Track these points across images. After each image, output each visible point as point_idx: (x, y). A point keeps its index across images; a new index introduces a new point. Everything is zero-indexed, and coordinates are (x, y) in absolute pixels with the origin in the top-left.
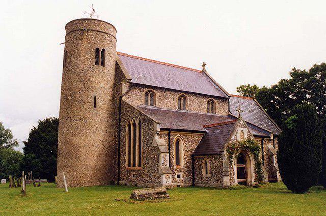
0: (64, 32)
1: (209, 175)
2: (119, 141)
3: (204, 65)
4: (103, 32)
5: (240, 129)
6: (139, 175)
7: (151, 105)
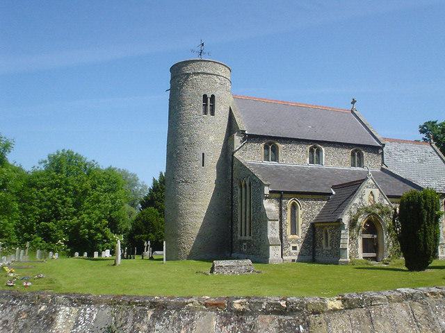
1: (330, 248)
3: (354, 102)
4: (211, 74)
5: (368, 191)
6: (249, 246)
7: (272, 161)
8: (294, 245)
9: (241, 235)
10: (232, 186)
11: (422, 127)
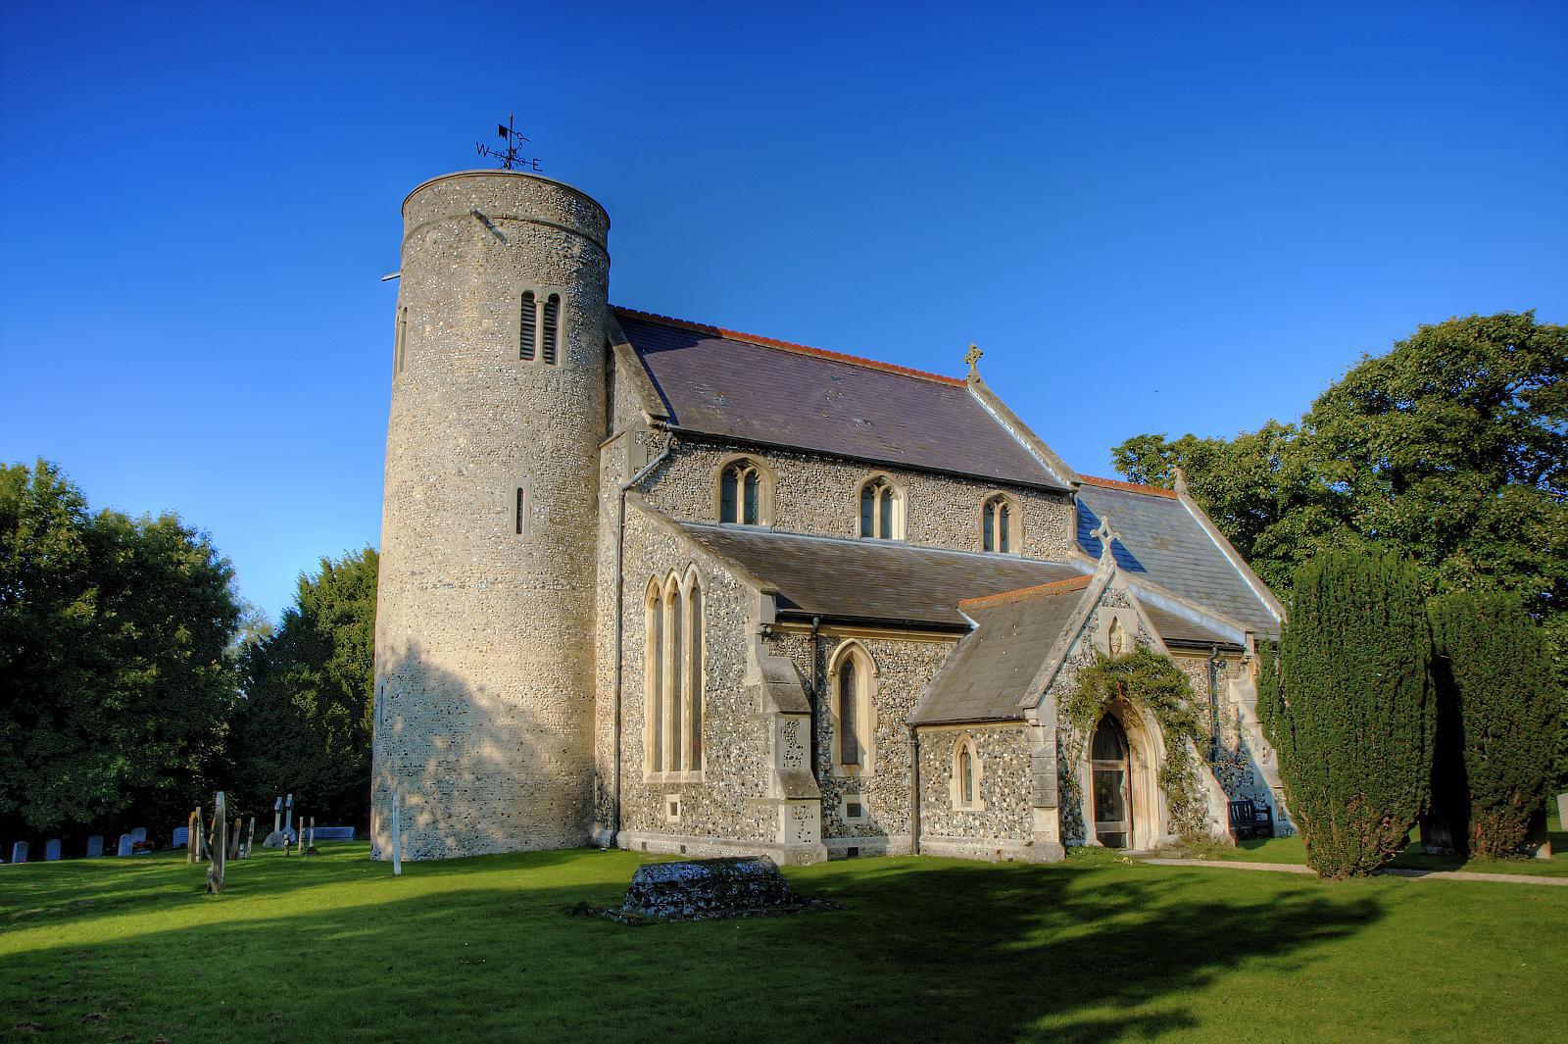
1: (978, 805)
9: (658, 767)
11: (1135, 445)
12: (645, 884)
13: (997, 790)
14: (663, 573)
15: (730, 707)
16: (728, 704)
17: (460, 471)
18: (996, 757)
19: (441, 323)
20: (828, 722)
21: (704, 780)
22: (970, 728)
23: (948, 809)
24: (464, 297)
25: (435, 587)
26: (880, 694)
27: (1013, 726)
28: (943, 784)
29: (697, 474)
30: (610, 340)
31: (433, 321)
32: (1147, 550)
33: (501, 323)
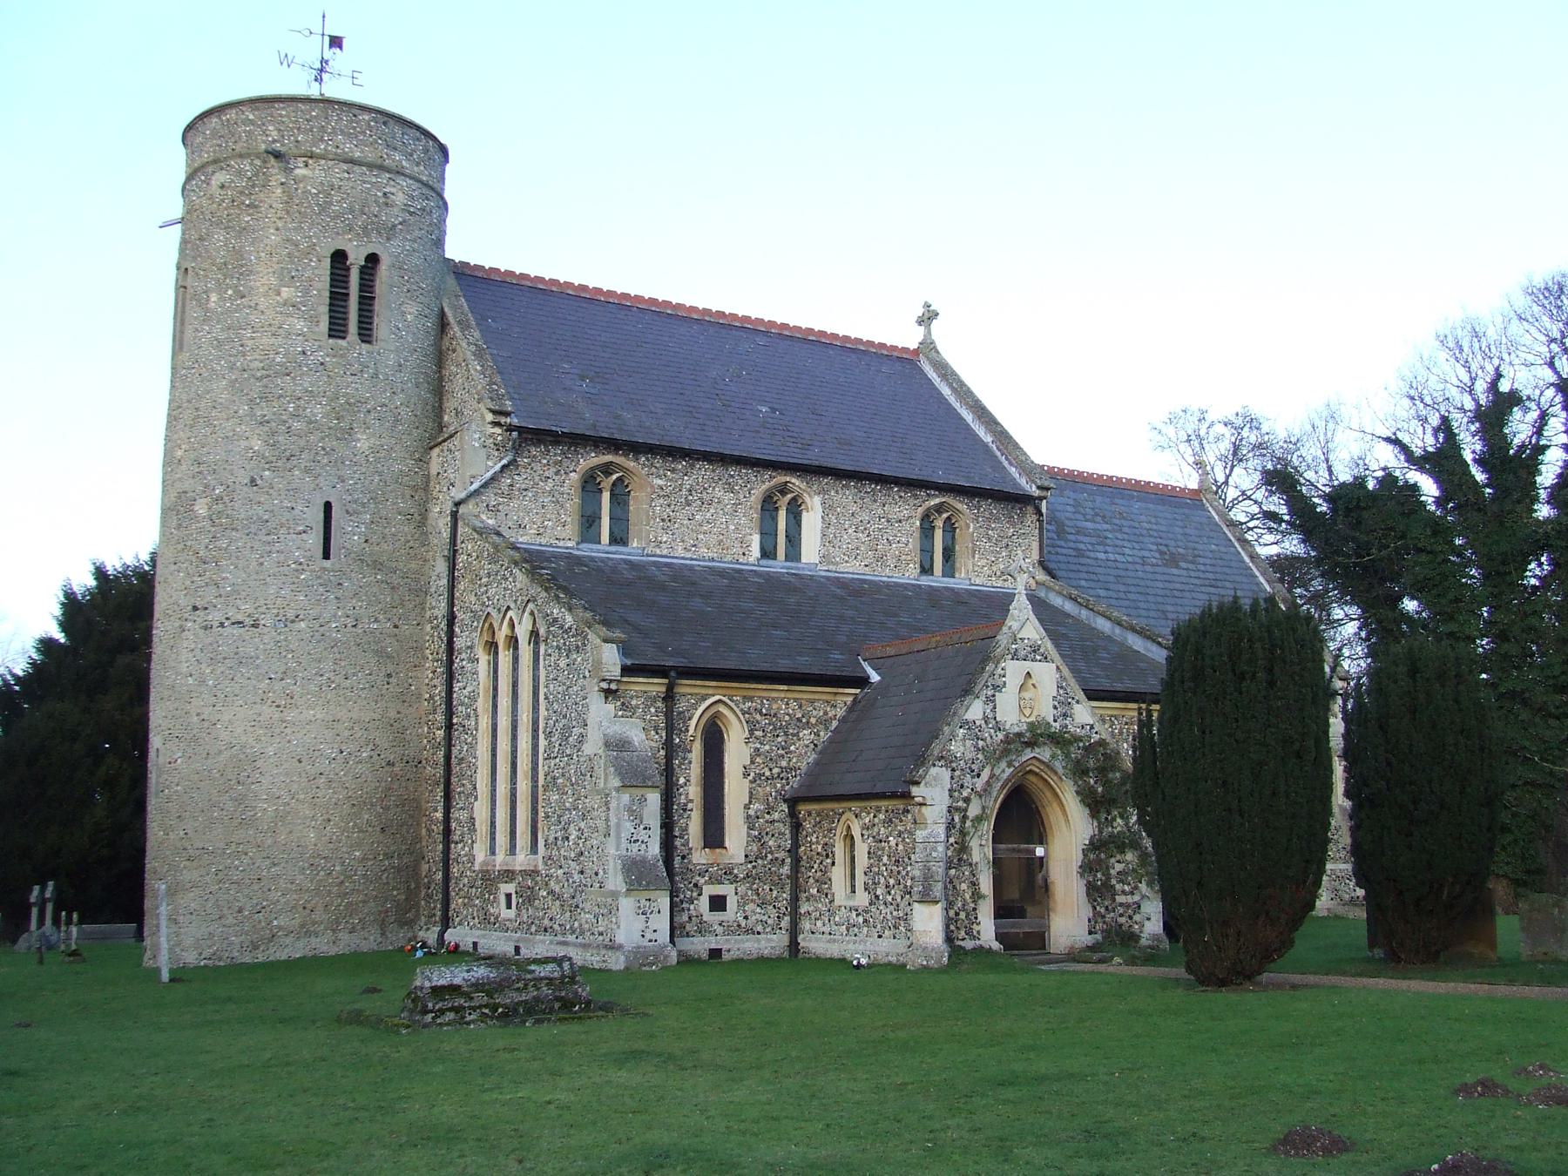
0: (176, 162)
1: (862, 899)
2: (449, 726)
3: (928, 317)
6: (528, 897)
8: (718, 890)
10: (450, 643)
12: (422, 988)
13: (882, 880)
14: (499, 610)
15: (569, 779)
16: (567, 775)
17: (253, 481)
18: (881, 841)
19: (230, 292)
20: (687, 797)
21: (541, 867)
22: (855, 805)
23: (830, 902)
24: (258, 258)
25: (222, 625)
26: (752, 762)
27: (899, 805)
28: (826, 872)
29: (550, 483)
30: (446, 310)
31: (221, 289)
32: (1148, 568)
33: (306, 292)
